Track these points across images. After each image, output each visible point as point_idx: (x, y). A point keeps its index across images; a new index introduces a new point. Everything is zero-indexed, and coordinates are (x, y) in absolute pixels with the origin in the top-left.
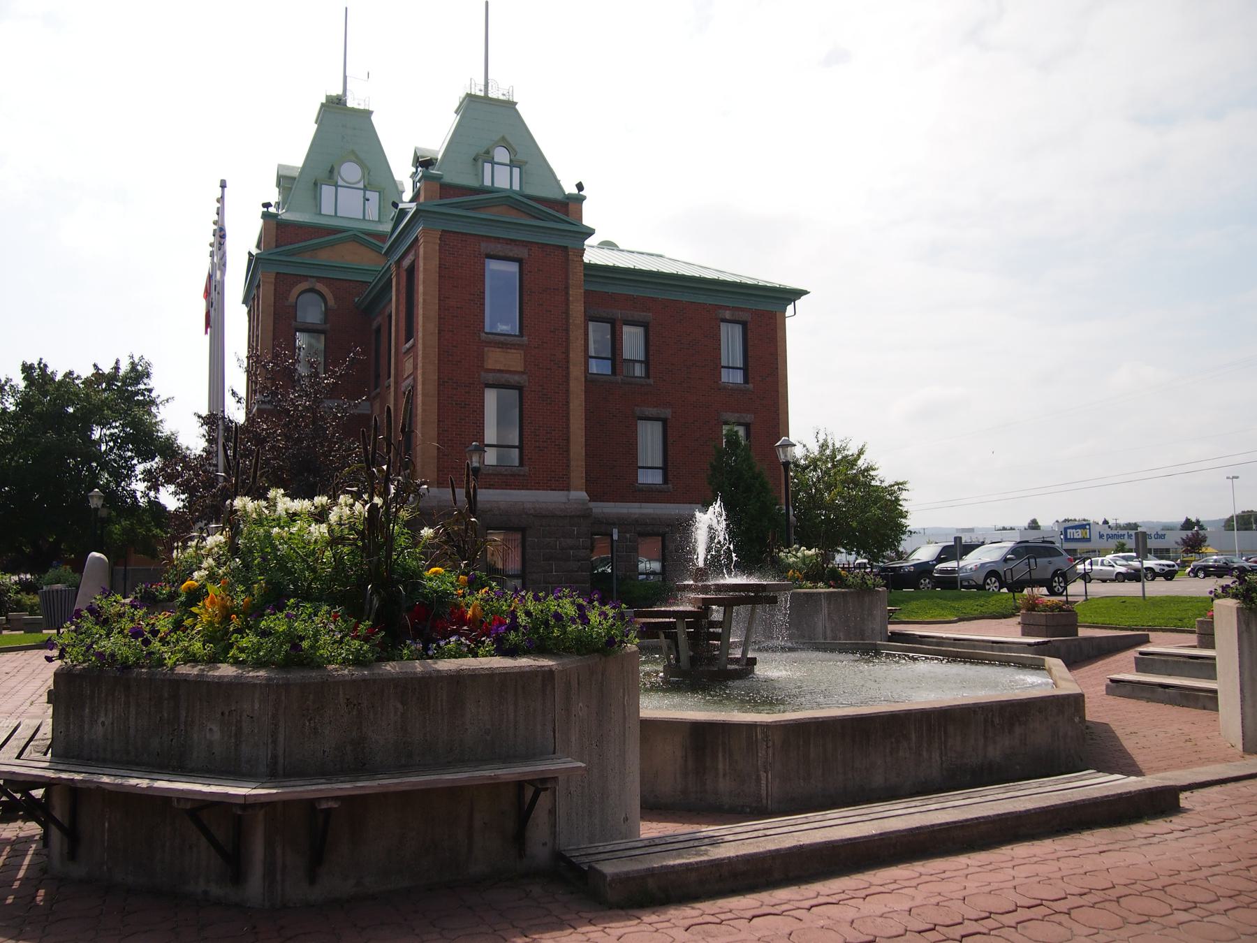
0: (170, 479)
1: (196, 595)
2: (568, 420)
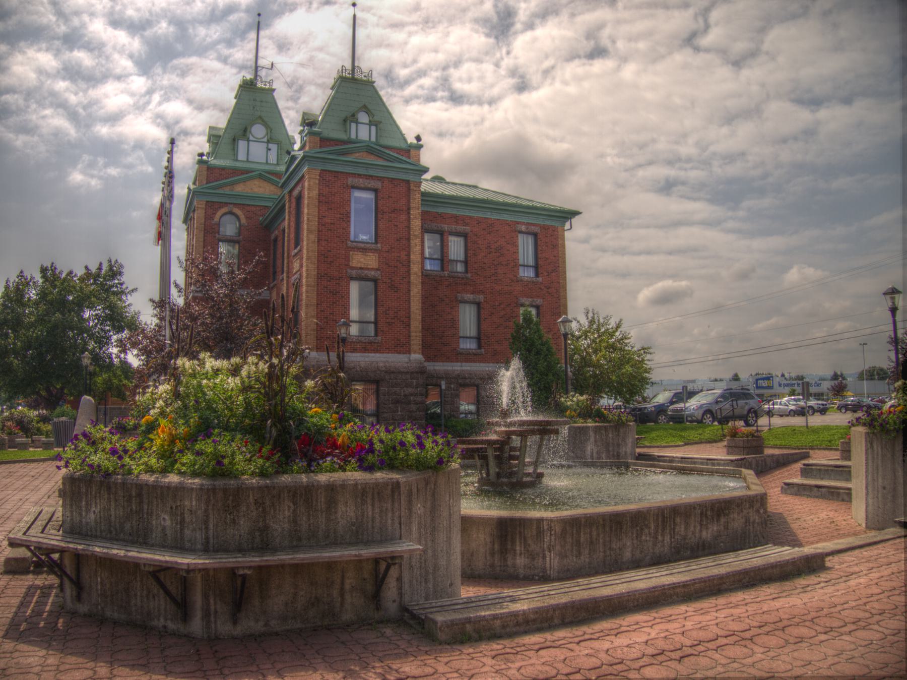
0: (134, 345)
1: (152, 427)
2: (409, 303)
